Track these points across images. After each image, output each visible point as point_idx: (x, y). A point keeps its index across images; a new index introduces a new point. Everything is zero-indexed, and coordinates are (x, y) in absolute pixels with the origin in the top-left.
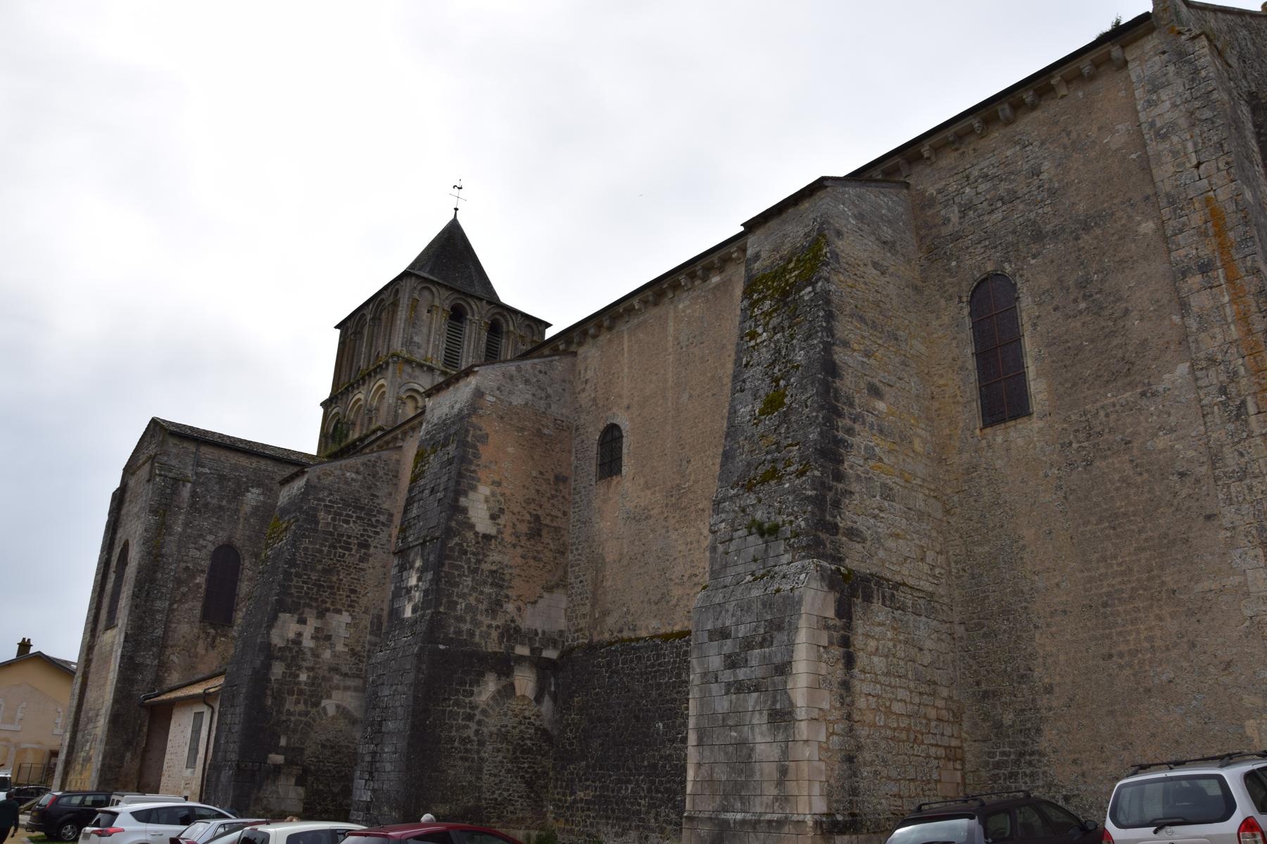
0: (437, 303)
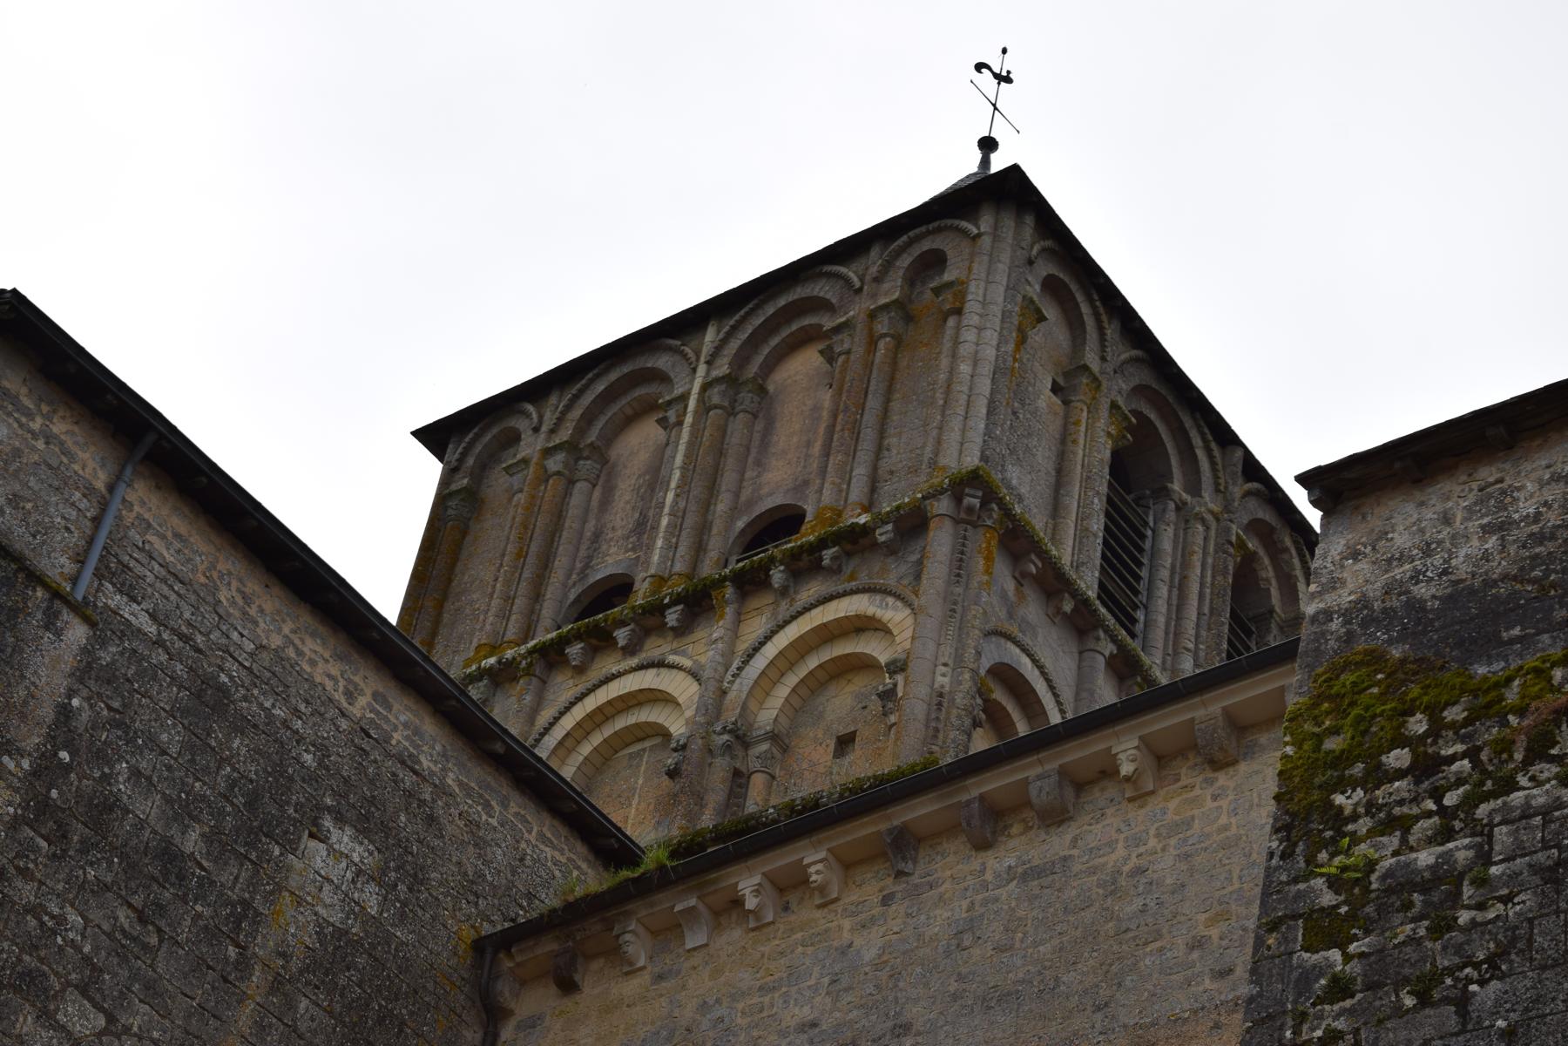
0: (1091, 359)
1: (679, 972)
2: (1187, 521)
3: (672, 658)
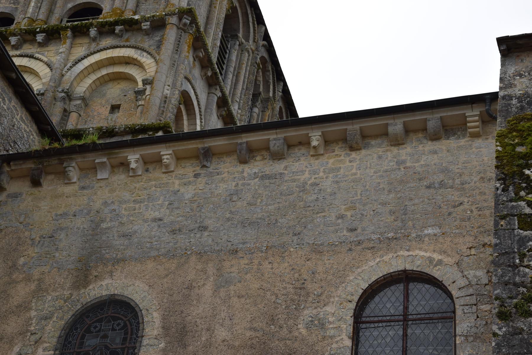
1: (93, 187)
2: (242, 51)
3: (37, 55)
